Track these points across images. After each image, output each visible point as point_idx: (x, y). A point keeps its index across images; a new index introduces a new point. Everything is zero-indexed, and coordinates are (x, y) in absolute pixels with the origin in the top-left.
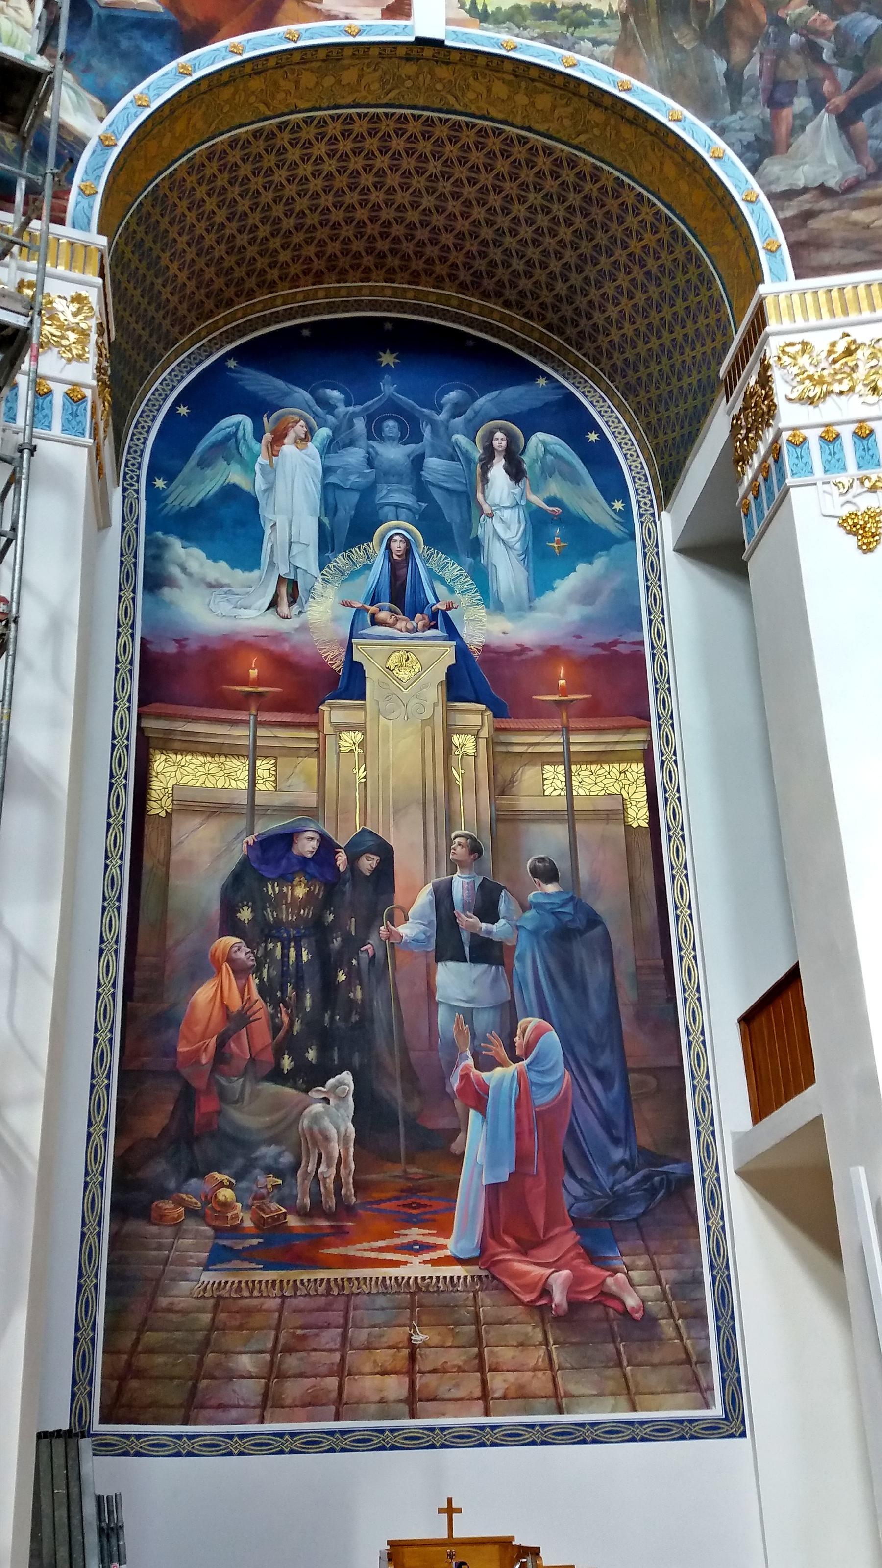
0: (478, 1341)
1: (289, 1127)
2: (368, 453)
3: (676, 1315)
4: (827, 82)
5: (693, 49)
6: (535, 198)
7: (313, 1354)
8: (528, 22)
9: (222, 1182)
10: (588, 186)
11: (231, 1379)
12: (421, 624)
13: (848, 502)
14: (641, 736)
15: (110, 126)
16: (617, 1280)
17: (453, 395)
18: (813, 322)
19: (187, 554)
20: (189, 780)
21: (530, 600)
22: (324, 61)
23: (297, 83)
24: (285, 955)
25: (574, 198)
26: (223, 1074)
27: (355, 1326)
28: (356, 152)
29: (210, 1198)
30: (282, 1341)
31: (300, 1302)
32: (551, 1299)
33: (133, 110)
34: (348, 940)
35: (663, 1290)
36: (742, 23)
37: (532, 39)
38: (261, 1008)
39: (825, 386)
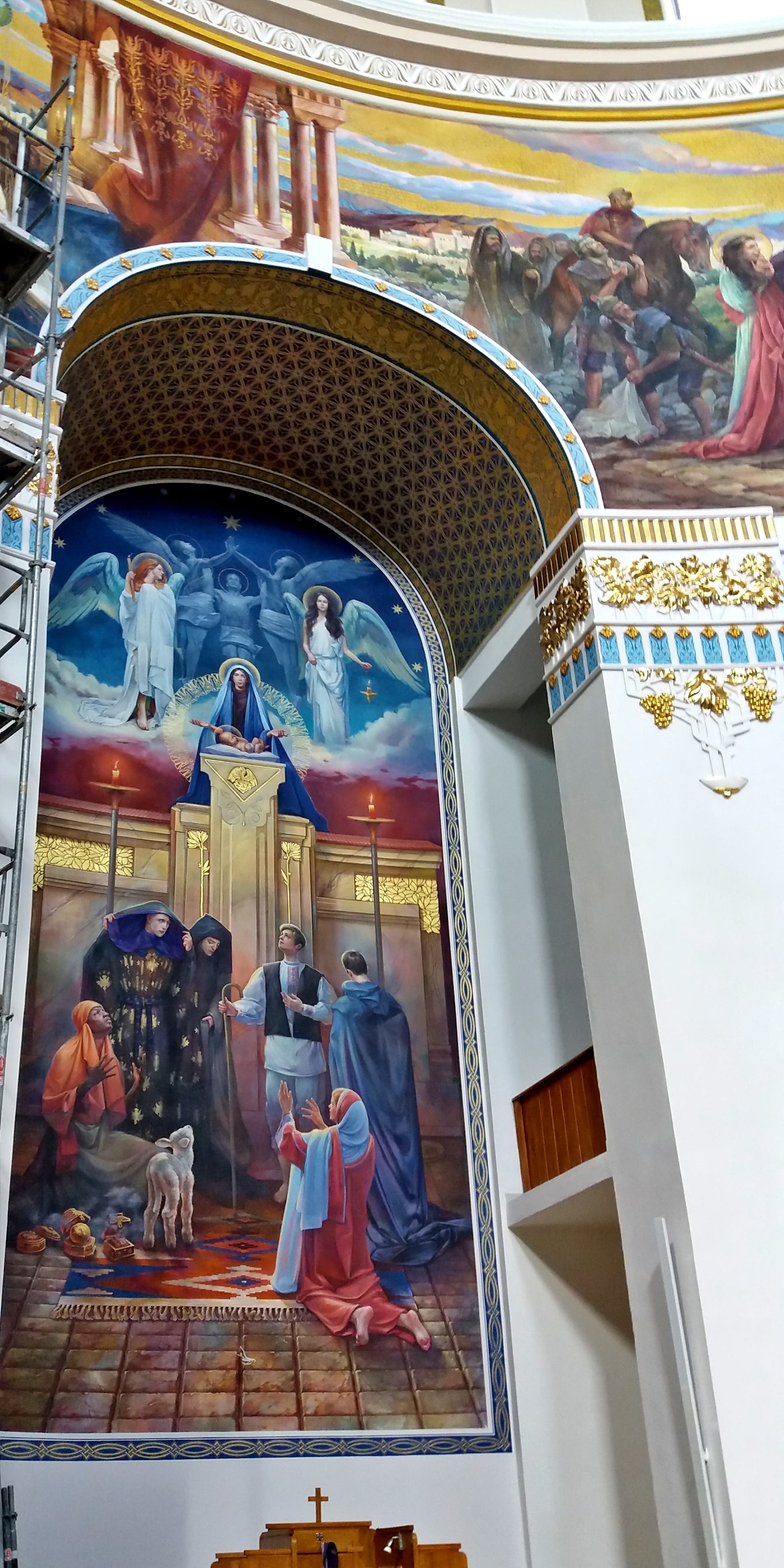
0: (294, 1365)
1: (137, 1172)
2: (215, 599)
3: (457, 1346)
4: (628, 357)
5: (525, 315)
6: (376, 411)
7: (154, 1372)
8: (396, 271)
9: (79, 1218)
10: (425, 409)
11: (83, 1392)
12: (257, 746)
13: (647, 687)
14: (435, 858)
15: (67, 301)
16: (409, 1316)
17: (285, 560)
18: (619, 543)
19: (61, 665)
20: (59, 861)
21: (347, 736)
22: (231, 275)
23: (206, 289)
24: (138, 1020)
25: (411, 417)
26: (81, 1122)
27: (191, 1349)
28: (238, 351)
29: (68, 1231)
30: (128, 1360)
31: (146, 1327)
32: (355, 1331)
33: (85, 291)
34: (191, 1010)
35: (447, 1326)
36: (563, 300)
37: (400, 285)
38: (115, 1065)
39: (629, 595)
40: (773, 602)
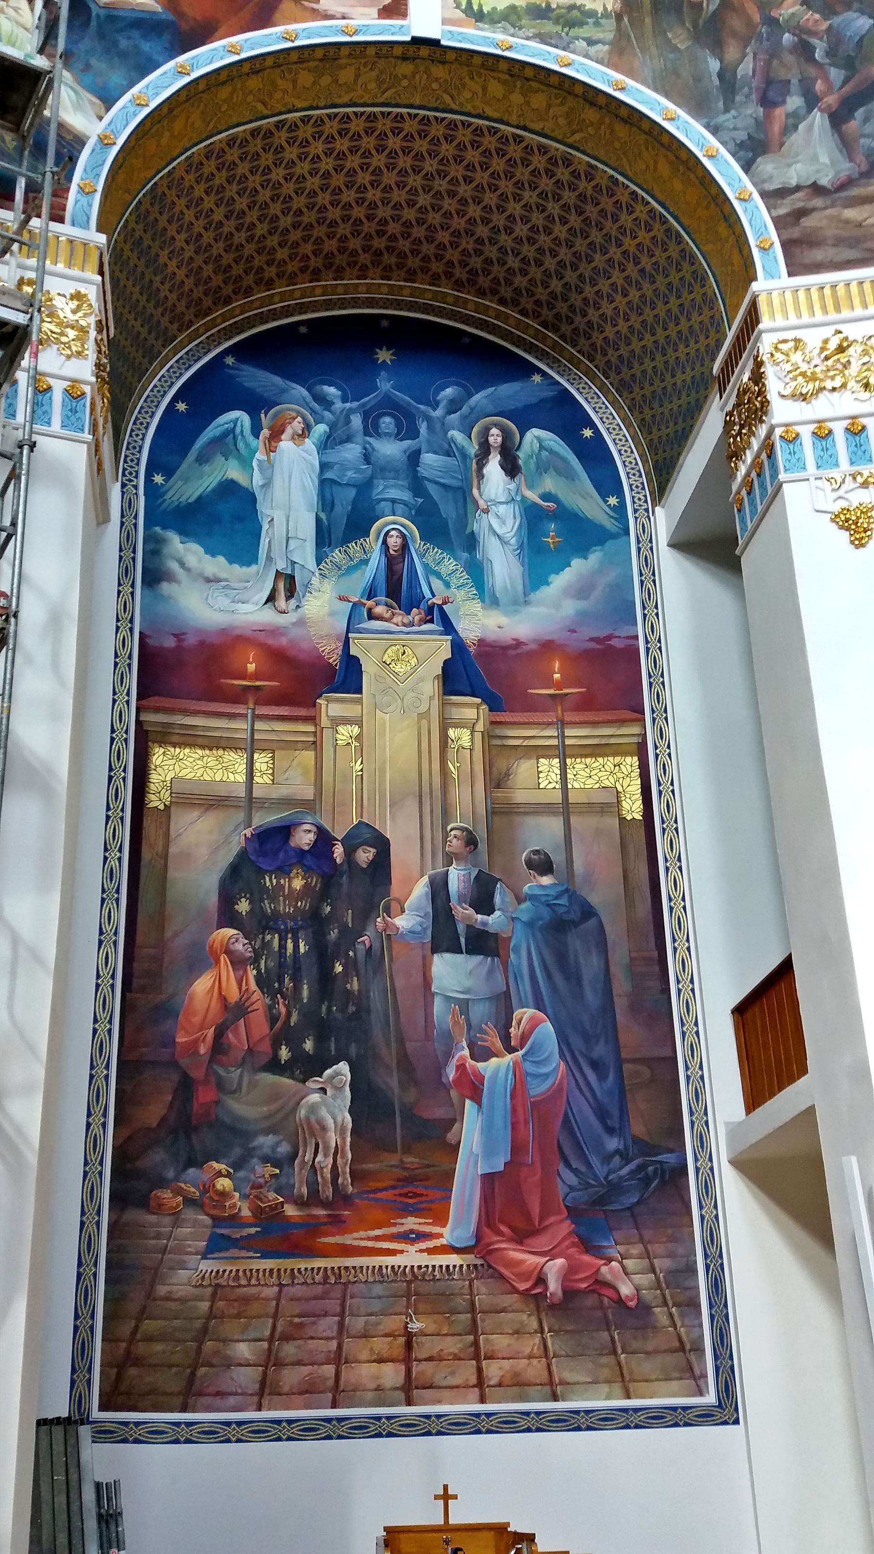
0: (474, 1329)
1: (287, 1117)
2: (365, 449)
3: (670, 1304)
4: (819, 82)
5: (687, 48)
6: (530, 196)
7: (310, 1342)
8: (524, 22)
10: (583, 185)
11: (229, 1366)
12: (417, 618)
13: (840, 498)
14: (635, 730)
15: (109, 124)
16: (611, 1269)
17: (449, 391)
18: (806, 319)
19: (186, 550)
20: (187, 773)
21: (526, 594)
22: (321, 60)
23: (294, 82)
24: (283, 947)
25: (569, 197)
26: (221, 1064)
27: (352, 1314)
28: (353, 150)
29: (208, 1188)
30: (279, 1329)
31: (297, 1291)
32: (546, 1288)
33: (132, 109)
34: (344, 931)
35: (657, 1279)
36: (735, 22)
37: (528, 38)
38: (258, 999)
39: (817, 383)
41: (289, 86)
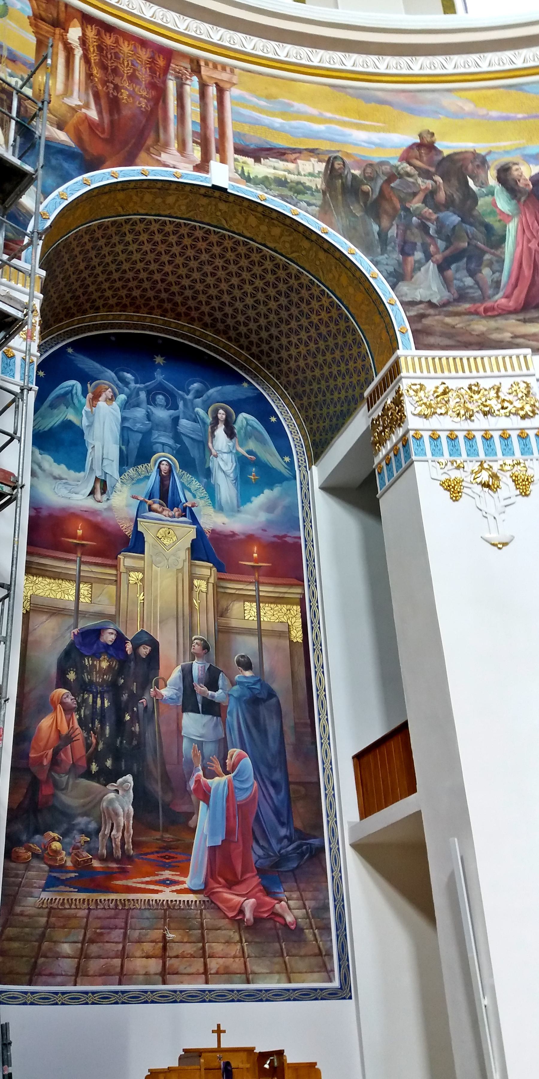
0: (202, 939)
1: (94, 806)
2: (148, 412)
3: (314, 926)
4: (432, 246)
5: (361, 216)
6: (259, 283)
7: (106, 944)
8: (272, 187)
10: (292, 281)
11: (57, 958)
12: (177, 513)
13: (445, 473)
14: (299, 590)
15: (46, 207)
16: (281, 906)
17: (196, 386)
18: (425, 374)
19: (42, 458)
20: (40, 592)
21: (238, 507)
22: (159, 189)
23: (142, 199)
24: (95, 702)
25: (282, 287)
26: (56, 772)
27: (131, 928)
28: (163, 242)
29: (46, 847)
30: (88, 936)
31: (100, 913)
32: (244, 916)
33: (58, 200)
34: (132, 695)
35: (307, 912)
36: (387, 206)
37: (275, 196)
38: (79, 733)
39: (432, 409)
40: (531, 414)
41: (243, 220)
